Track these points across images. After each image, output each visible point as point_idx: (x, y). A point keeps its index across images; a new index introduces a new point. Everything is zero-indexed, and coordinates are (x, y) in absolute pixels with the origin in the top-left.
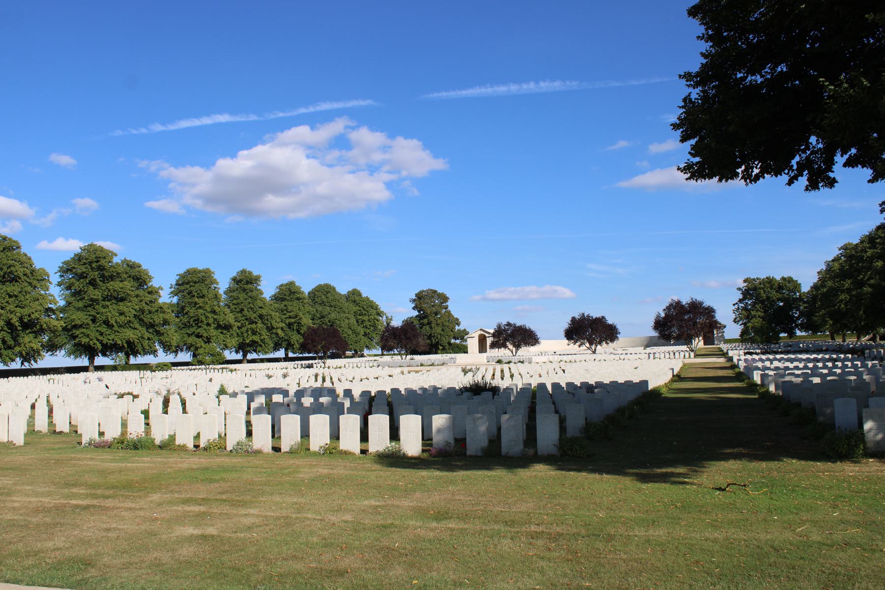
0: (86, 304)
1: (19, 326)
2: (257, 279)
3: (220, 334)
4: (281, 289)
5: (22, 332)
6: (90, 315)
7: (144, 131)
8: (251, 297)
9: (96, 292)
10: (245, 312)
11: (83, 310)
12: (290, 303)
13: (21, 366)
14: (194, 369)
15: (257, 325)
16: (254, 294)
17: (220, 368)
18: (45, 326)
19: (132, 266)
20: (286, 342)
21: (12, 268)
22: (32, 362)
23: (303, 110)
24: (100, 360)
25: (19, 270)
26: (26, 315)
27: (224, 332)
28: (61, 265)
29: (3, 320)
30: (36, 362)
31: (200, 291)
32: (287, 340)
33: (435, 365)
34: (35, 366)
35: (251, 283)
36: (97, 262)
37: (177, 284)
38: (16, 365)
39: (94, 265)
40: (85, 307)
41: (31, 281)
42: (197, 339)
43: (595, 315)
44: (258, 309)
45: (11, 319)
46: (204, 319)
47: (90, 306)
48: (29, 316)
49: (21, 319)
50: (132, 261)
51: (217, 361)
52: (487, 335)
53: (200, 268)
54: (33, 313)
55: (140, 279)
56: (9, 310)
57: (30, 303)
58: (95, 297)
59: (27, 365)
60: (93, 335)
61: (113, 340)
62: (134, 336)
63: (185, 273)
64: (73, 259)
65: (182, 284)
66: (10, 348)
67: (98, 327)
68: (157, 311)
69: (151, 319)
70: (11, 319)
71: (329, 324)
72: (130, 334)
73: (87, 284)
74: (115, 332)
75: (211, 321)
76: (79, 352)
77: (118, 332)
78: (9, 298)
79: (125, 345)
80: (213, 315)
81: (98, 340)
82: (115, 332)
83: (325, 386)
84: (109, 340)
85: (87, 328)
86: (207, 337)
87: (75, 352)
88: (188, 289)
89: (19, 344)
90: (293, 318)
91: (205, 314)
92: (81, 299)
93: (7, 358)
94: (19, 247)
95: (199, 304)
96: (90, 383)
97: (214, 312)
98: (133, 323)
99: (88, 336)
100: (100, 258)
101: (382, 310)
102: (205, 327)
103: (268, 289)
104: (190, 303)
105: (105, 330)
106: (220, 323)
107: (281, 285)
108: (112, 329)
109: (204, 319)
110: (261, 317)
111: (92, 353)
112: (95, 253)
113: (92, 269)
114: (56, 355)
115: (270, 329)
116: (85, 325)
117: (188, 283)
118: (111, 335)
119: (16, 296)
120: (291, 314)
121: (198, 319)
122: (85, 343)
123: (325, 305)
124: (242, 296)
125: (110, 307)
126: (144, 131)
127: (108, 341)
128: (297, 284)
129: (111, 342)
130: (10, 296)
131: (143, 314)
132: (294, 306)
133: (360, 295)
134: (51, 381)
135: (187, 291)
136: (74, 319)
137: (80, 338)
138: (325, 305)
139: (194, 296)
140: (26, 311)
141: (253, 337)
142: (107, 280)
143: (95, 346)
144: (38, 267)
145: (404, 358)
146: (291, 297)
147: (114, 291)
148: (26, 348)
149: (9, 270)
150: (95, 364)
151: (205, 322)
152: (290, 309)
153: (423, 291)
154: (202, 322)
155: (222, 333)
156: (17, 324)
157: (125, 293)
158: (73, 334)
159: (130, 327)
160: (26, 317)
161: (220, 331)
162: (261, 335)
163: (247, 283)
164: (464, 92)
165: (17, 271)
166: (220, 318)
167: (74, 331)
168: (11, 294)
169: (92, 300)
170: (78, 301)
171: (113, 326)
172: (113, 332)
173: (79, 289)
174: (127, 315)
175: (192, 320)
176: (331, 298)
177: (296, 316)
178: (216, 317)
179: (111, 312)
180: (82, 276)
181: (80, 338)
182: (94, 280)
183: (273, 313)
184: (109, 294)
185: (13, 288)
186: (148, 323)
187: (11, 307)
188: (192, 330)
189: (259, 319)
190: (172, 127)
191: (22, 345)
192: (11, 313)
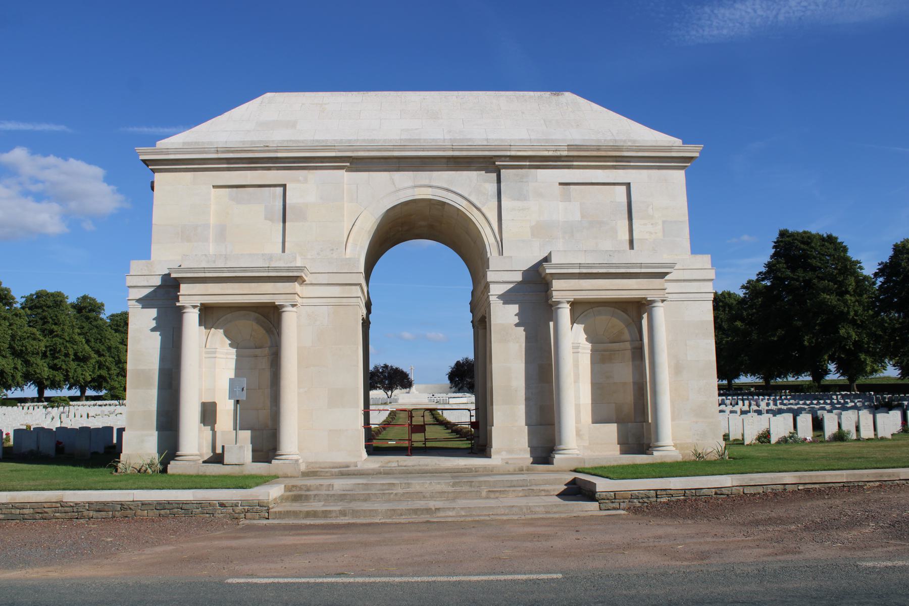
8: (97, 327)
17: (36, 405)
27: (82, 364)
35: (94, 311)
44: (107, 341)
50: (34, 293)
53: (51, 290)
63: (32, 295)
69: (22, 347)
75: (71, 352)
83: (62, 426)
91: (63, 344)
102: (63, 358)
106: (78, 354)
107: (112, 315)
124: (86, 325)
141: (100, 371)
155: (79, 365)
161: (76, 363)
162: (109, 369)
163: (90, 311)
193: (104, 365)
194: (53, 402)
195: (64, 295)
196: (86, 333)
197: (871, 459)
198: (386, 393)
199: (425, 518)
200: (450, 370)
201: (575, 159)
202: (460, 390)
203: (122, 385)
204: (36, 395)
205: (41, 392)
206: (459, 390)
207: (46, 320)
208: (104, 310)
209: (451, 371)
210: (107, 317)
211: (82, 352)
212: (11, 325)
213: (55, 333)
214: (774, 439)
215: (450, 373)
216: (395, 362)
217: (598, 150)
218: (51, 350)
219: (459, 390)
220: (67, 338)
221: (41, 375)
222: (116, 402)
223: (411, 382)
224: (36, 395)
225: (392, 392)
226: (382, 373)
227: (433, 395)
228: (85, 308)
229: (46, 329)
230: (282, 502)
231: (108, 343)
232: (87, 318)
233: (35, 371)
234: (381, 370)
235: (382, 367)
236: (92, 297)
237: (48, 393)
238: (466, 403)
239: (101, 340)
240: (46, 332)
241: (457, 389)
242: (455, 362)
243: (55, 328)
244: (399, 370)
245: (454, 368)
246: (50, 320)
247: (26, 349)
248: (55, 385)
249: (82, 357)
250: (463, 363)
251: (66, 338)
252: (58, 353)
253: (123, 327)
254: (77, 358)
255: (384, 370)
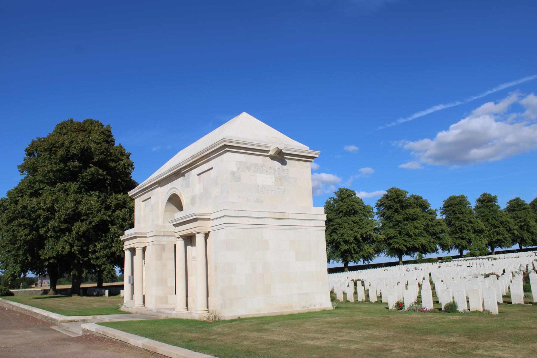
8: (493, 211)
27: (479, 235)
35: (491, 201)
53: (457, 195)
75: (470, 228)
141: (498, 237)
155: (478, 235)
161: (476, 234)
162: (503, 235)
194: (443, 259)
197: (194, 331)
201: (197, 162)
204: (519, 248)
213: (460, 219)
214: (407, 306)
217: (198, 155)
218: (459, 229)
221: (447, 244)
222: (475, 257)
224: (519, 248)
240: (456, 219)
243: (461, 216)
247: (436, 231)
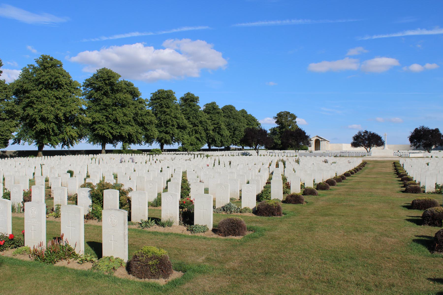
0: (102, 108)
1: (63, 119)
2: (197, 98)
3: (180, 132)
4: (207, 107)
5: (64, 124)
6: (104, 115)
7: (98, 40)
9: (109, 100)
10: (191, 119)
11: (99, 112)
12: (214, 116)
13: (62, 148)
14: (183, 154)
15: (199, 127)
16: (196, 107)
17: (199, 154)
18: (80, 120)
19: (129, 85)
20: (212, 139)
21: (58, 79)
22: (70, 146)
23: (175, 31)
24: (109, 146)
25: (63, 81)
26: (68, 112)
27: (182, 131)
28: (85, 82)
29: (53, 114)
30: (72, 145)
31: (167, 104)
32: (212, 138)
33: (338, 157)
34: (72, 148)
35: (193, 101)
36: (109, 80)
37: (151, 100)
38: (59, 147)
39: (107, 82)
40: (101, 109)
41: (70, 89)
42: (166, 135)
43: (432, 127)
44: (199, 117)
45: (58, 114)
46: (170, 122)
47: (104, 109)
48: (70, 112)
49: (64, 115)
51: (196, 148)
52: (320, 140)
53: (166, 89)
54: (73, 111)
55: (134, 93)
56: (57, 108)
57: (70, 103)
58: (108, 103)
59: (66, 148)
60: (107, 128)
61: (120, 133)
62: (133, 131)
63: (156, 92)
64: (92, 78)
65: (155, 99)
66: (56, 135)
67: (109, 123)
68: (146, 115)
69: (142, 120)
70: (58, 114)
71: (233, 129)
72: (129, 129)
73: (102, 94)
74: (121, 128)
75: (175, 123)
76: (96, 140)
77: (123, 127)
78: (56, 99)
79: (127, 136)
80: (176, 120)
81: (110, 132)
82: (121, 128)
84: (117, 132)
85: (103, 124)
86: (172, 134)
87: (94, 140)
88: (159, 102)
89: (62, 133)
90: (216, 125)
91: (171, 119)
92: (97, 105)
93: (55, 142)
94: (61, 66)
95: (167, 112)
96: (125, 162)
97: (176, 117)
98: (131, 122)
99: (103, 129)
100: (111, 77)
101: (259, 122)
102: (171, 127)
103: (202, 105)
104: (161, 112)
105: (114, 126)
107: (207, 104)
108: (119, 125)
109: (170, 122)
110: (201, 122)
111: (103, 140)
112: (107, 74)
113: (106, 84)
114: (81, 142)
115: (206, 130)
116: (102, 122)
117: (158, 99)
118: (118, 129)
119: (60, 99)
120: (215, 122)
121: (166, 122)
122: (101, 134)
123: (230, 118)
124: (189, 109)
125: (117, 110)
126: (98, 40)
127: (116, 133)
128: (217, 104)
129: (118, 134)
130: (57, 99)
131: (137, 116)
132: (216, 117)
133: (246, 113)
134: (94, 160)
135: (159, 103)
136: (95, 118)
137: (98, 131)
138: (230, 118)
139: (163, 107)
140: (68, 109)
142: (115, 92)
143: (108, 136)
144: (74, 80)
145: (297, 151)
146: (213, 111)
147: (120, 100)
148: (68, 135)
149: (56, 80)
150: (106, 149)
151: (171, 124)
152: (214, 118)
153: (282, 112)
154: (169, 123)
155: (181, 131)
156: (62, 118)
157: (127, 101)
158: (93, 128)
159: (130, 125)
160: (68, 113)
161: (179, 130)
162: (200, 133)
163: (191, 101)
164: (253, 24)
165: (61, 81)
166: (180, 121)
167: (94, 126)
168: (57, 96)
169: (105, 105)
170: (96, 105)
171: (119, 123)
172: (120, 127)
173: (97, 97)
174: (128, 116)
175: (162, 122)
176: (234, 113)
177: (218, 123)
178: (177, 121)
179: (119, 113)
180: (98, 89)
181: (98, 131)
182: (107, 92)
183: (208, 121)
184: (117, 102)
185: (58, 92)
186: (140, 123)
187: (58, 106)
188: (163, 129)
189: (200, 124)
190: (111, 38)
191: (65, 133)
192: (58, 110)
193: (198, 132)
195: (173, 92)
196: (189, 113)
198: (366, 149)
199: (261, 222)
200: (410, 135)
202: (417, 148)
203: (189, 142)
205: (162, 146)
206: (417, 148)
207: (162, 106)
208: (199, 100)
209: (411, 135)
210: (204, 105)
211: (182, 124)
212: (136, 108)
213: (166, 113)
215: (410, 136)
216: (373, 130)
219: (417, 148)
220: (173, 116)
223: (383, 142)
225: (370, 149)
226: (363, 136)
227: (398, 151)
228: (188, 99)
229: (162, 111)
230: (26, 200)
231: (200, 119)
232: (190, 105)
233: (150, 134)
234: (363, 134)
235: (364, 132)
236: (192, 93)
237: (166, 147)
238: (422, 157)
239: (196, 117)
240: (162, 113)
241: (415, 147)
242: (414, 129)
244: (375, 134)
245: (414, 133)
246: (164, 106)
247: (144, 122)
248: (167, 142)
249: (182, 127)
250: (420, 129)
251: (172, 116)
252: (168, 124)
253: (213, 110)
254: (179, 127)
255: (365, 134)
